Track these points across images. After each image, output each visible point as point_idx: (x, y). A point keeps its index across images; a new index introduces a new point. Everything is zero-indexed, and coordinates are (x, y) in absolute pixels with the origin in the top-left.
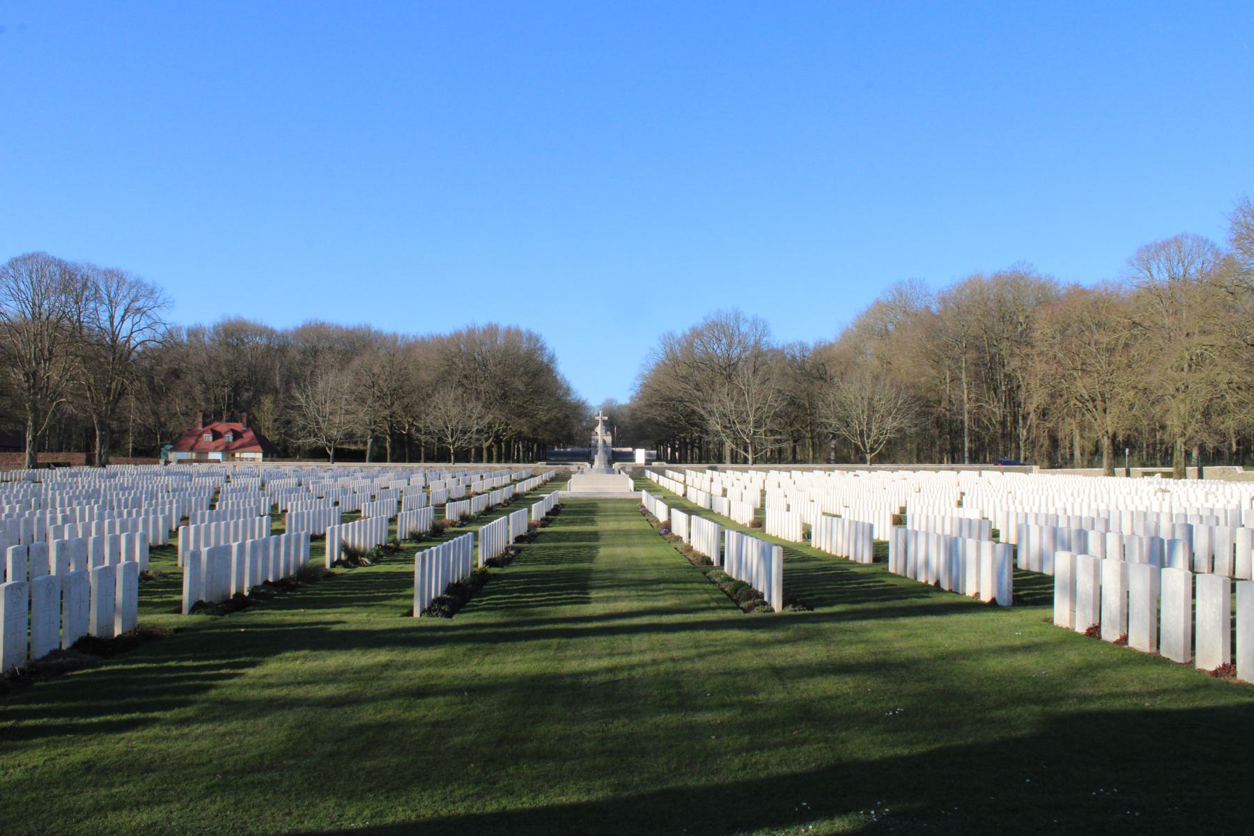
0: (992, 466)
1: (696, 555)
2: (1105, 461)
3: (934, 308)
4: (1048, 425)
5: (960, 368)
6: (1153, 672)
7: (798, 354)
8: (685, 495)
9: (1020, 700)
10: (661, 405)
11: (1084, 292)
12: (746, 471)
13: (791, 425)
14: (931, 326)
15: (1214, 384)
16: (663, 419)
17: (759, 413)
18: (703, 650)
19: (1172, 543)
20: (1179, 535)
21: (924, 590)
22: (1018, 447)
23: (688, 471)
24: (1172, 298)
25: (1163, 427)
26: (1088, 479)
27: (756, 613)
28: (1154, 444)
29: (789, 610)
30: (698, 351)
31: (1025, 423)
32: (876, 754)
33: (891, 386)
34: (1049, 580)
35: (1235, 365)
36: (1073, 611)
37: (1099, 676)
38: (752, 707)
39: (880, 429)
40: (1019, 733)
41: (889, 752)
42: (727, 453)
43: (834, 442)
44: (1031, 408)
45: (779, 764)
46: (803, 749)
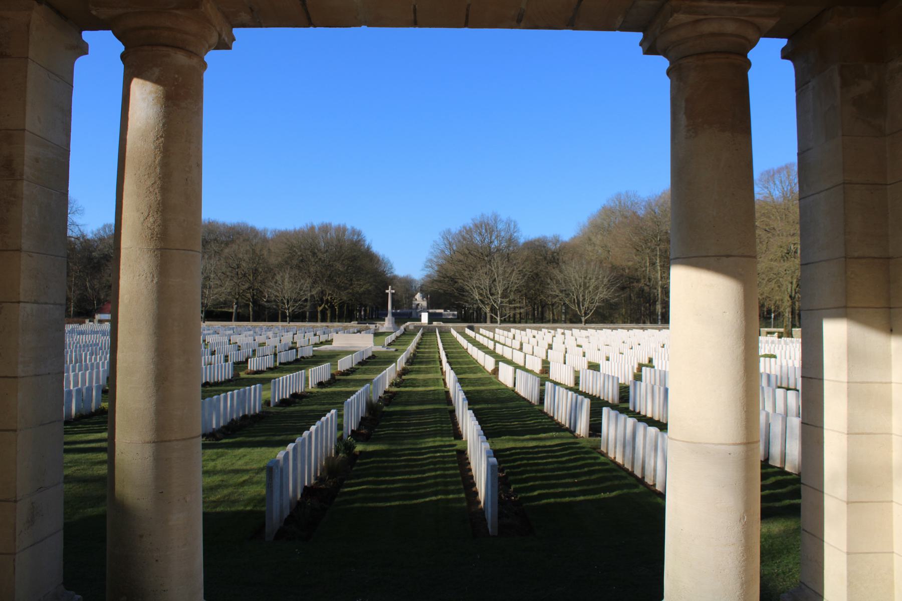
23: (497, 330)
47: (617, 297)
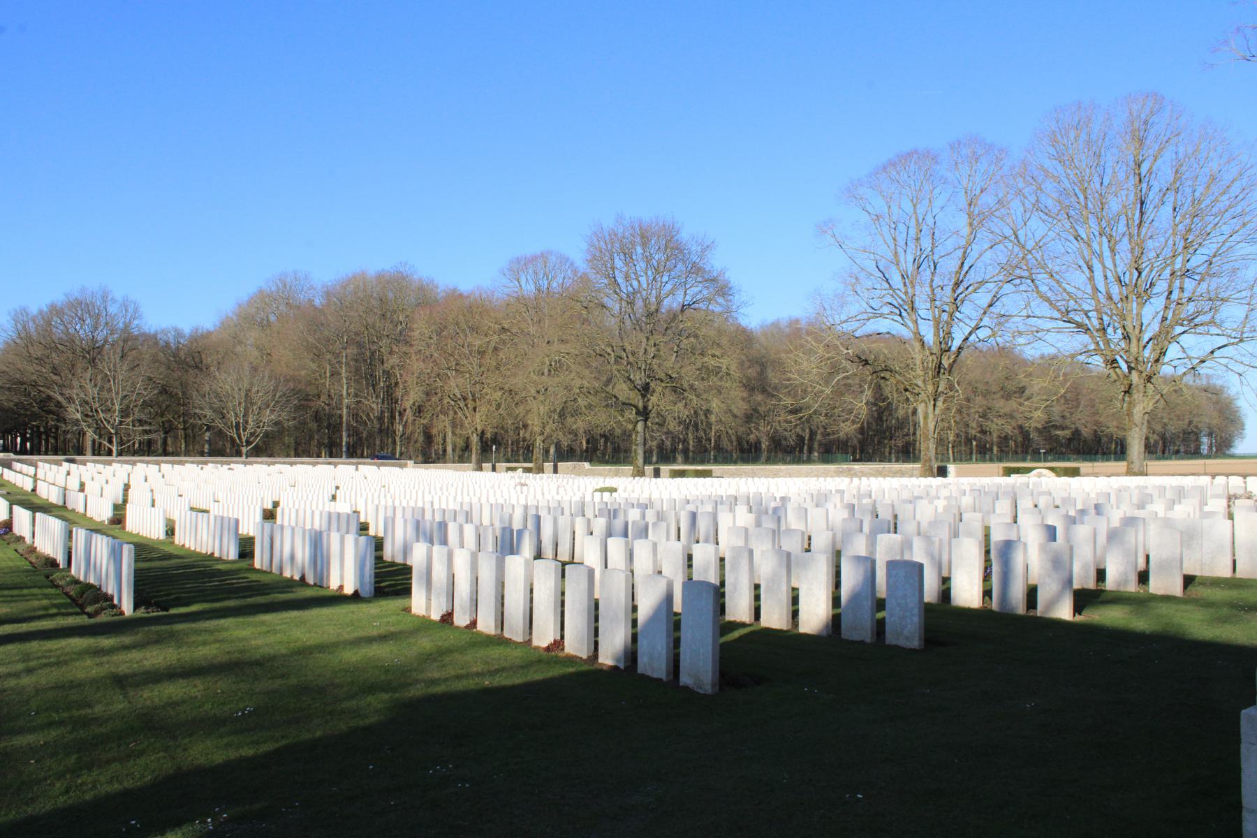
0: (369, 460)
1: (40, 557)
2: (474, 457)
3: (317, 302)
4: (423, 421)
5: (340, 363)
6: (495, 652)
7: (171, 340)
8: (34, 490)
9: (372, 688)
10: (9, 389)
11: (461, 295)
12: (110, 463)
13: (162, 416)
14: (313, 319)
15: (568, 388)
16: (11, 405)
17: (126, 402)
18: (32, 664)
19: (520, 532)
20: (530, 525)
21: (290, 584)
22: (394, 442)
23: (40, 464)
24: (538, 309)
25: (525, 426)
26: (458, 473)
27: (103, 618)
28: (518, 442)
29: (141, 613)
30: (58, 332)
31: (401, 419)
32: (219, 758)
33: (270, 377)
34: (406, 570)
35: (587, 372)
36: (429, 599)
37: (447, 659)
38: (85, 722)
39: (258, 422)
40: (367, 722)
41: (232, 754)
42: (89, 444)
43: (208, 434)
44: (408, 404)
45: (110, 782)
46: (138, 761)
47: (294, 419)
